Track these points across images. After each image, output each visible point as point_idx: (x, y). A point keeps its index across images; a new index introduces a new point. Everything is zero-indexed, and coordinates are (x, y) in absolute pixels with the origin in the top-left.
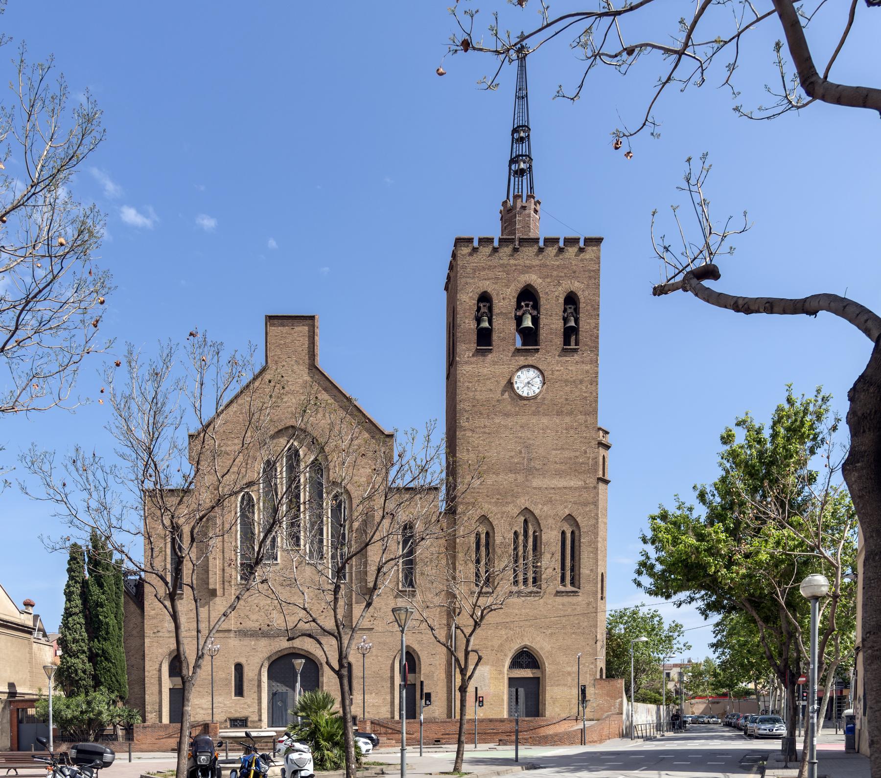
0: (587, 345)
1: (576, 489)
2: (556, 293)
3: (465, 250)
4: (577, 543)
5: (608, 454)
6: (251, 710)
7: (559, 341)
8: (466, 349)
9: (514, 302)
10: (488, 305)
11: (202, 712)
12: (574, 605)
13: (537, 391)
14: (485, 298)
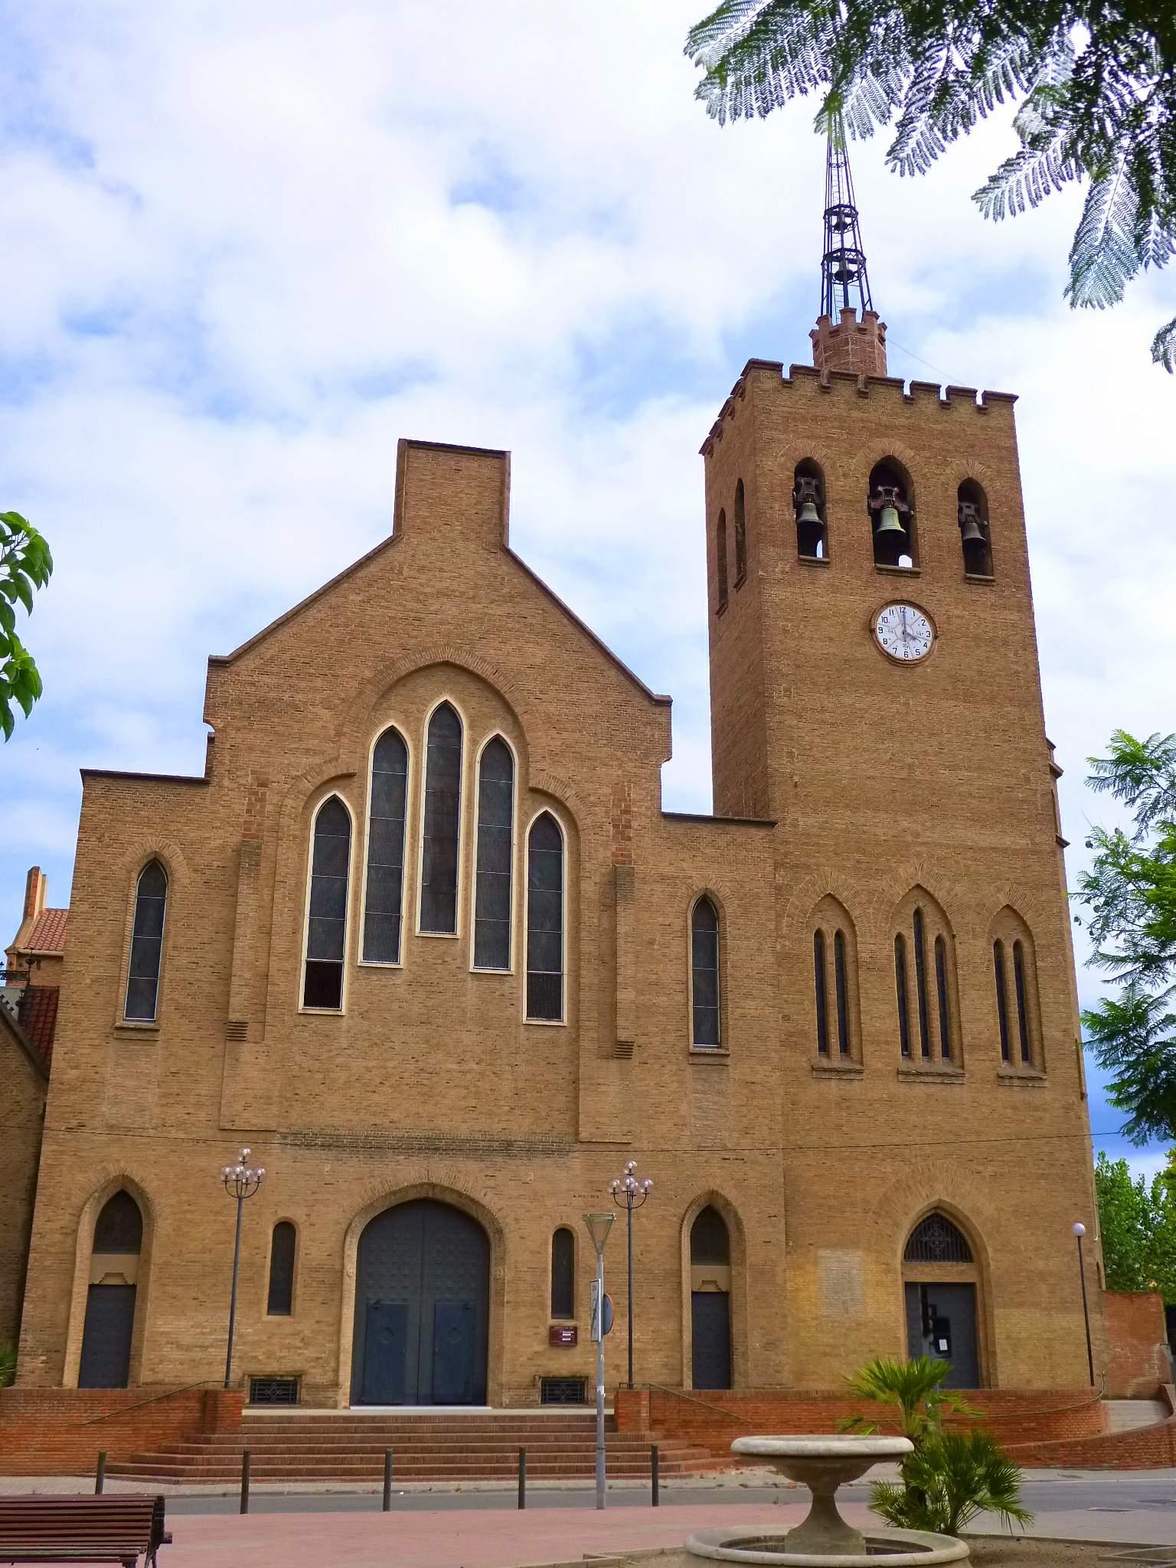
1: (1016, 852)
3: (767, 381)
4: (1029, 971)
6: (311, 1352)
7: (956, 562)
8: (776, 558)
9: (864, 483)
11: (177, 1355)
12: (1036, 1109)
13: (924, 651)
14: (807, 470)
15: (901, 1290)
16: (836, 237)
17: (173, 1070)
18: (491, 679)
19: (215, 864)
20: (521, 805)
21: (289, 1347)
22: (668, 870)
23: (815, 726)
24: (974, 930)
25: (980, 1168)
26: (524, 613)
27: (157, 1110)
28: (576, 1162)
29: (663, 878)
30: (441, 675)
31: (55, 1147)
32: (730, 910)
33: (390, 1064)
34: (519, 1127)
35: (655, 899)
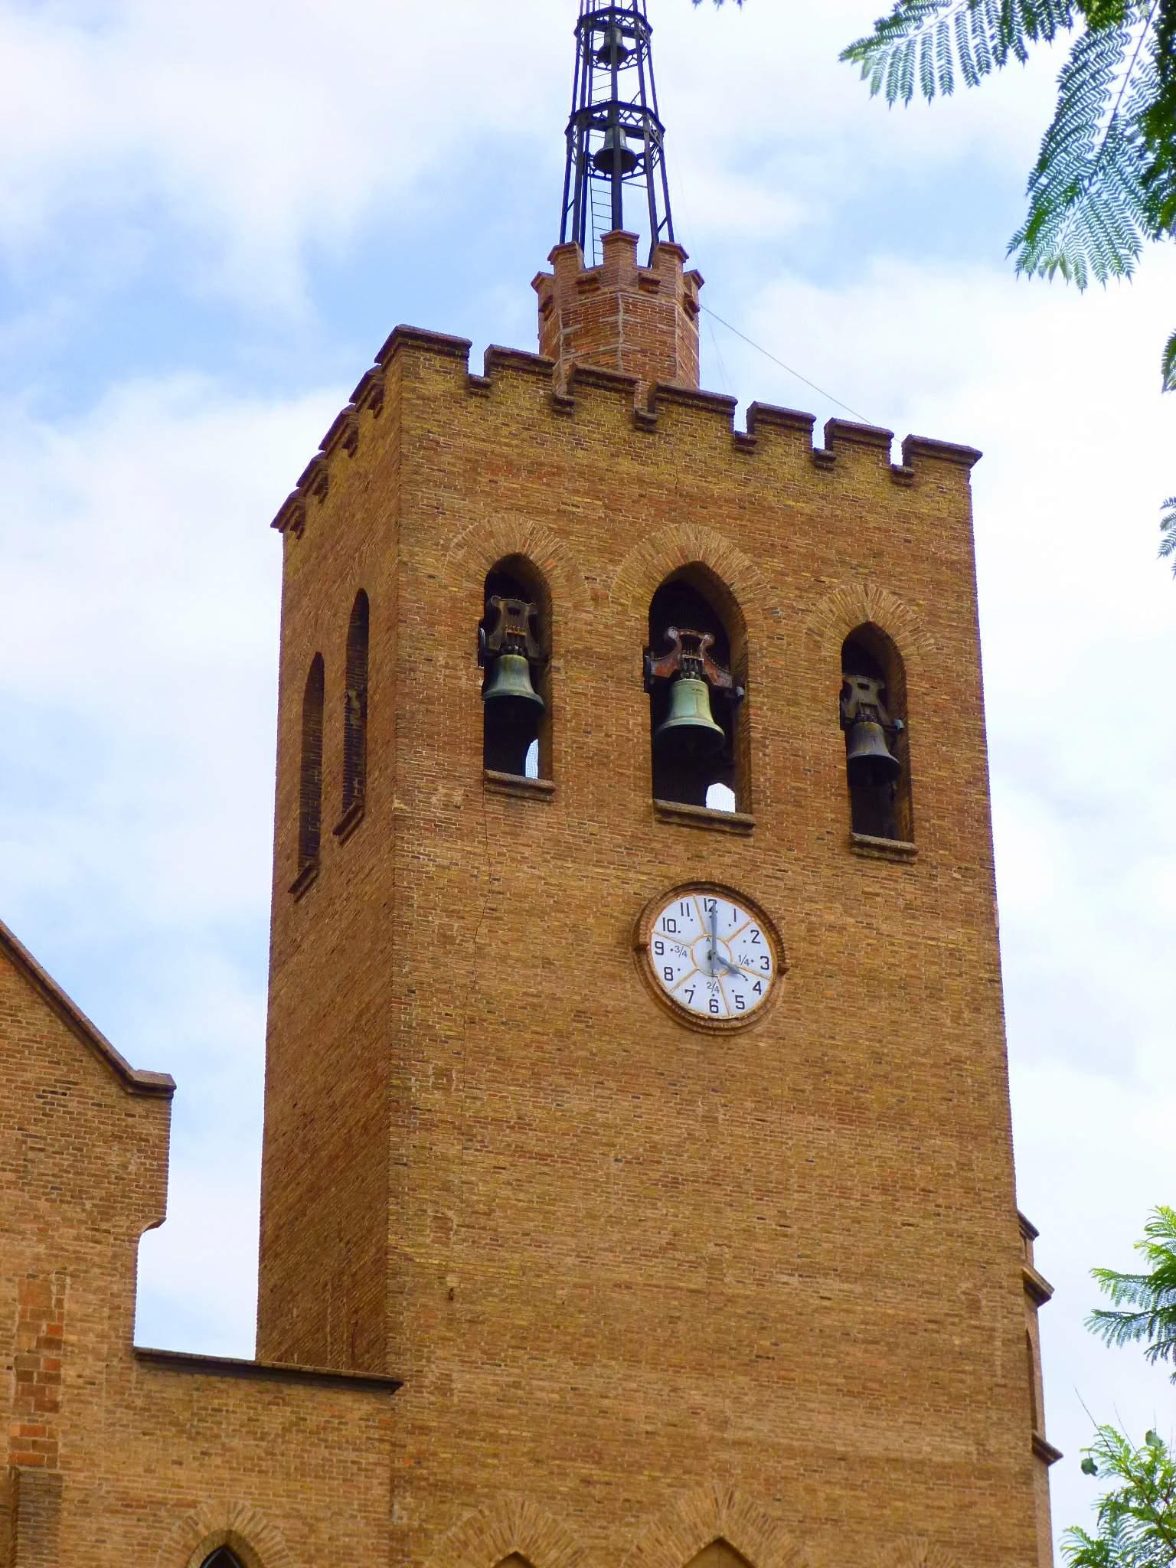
0: (943, 844)
1: (943, 1472)
2: (811, 620)
5: (1134, 1340)
7: (832, 808)
8: (432, 773)
9: (638, 618)
10: (527, 610)
13: (753, 1000)
14: (513, 581)
22: (139, 1486)
23: (502, 1160)
29: (128, 1504)
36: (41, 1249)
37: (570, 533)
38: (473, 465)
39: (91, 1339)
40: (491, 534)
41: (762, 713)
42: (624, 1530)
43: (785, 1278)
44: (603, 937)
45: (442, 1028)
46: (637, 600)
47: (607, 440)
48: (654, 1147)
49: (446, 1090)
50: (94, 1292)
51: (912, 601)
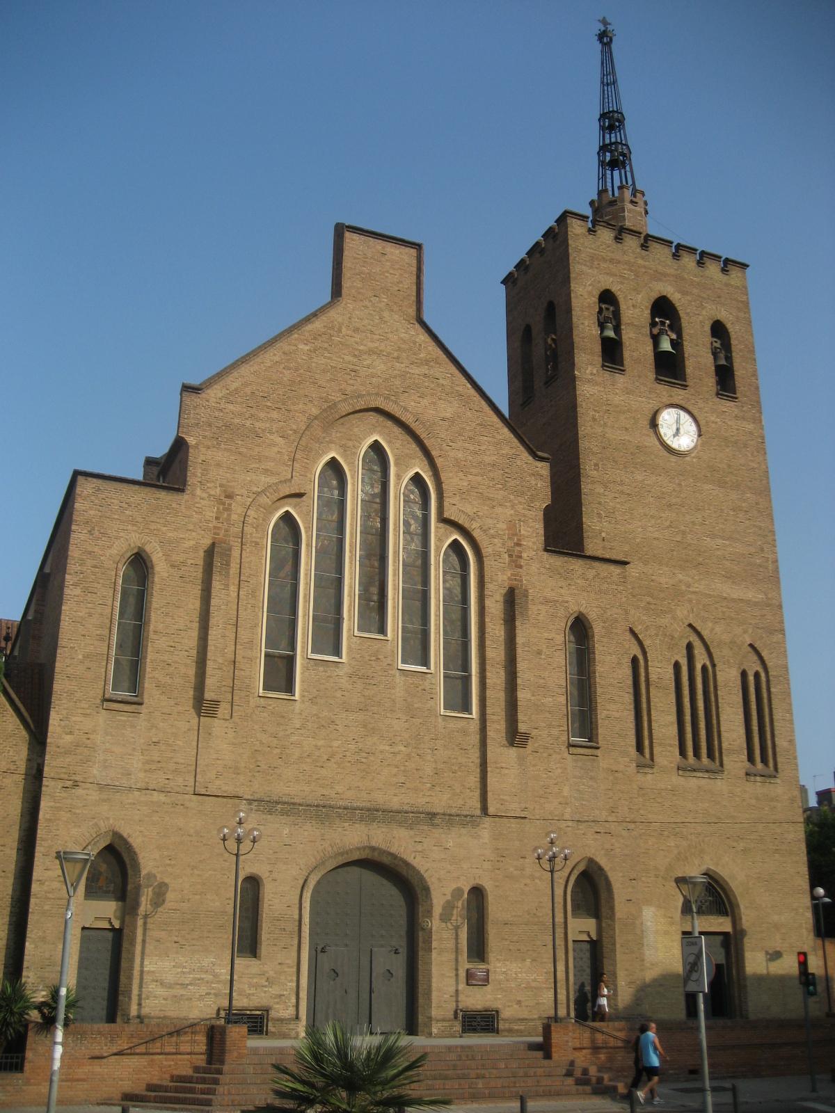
1: (756, 604)
6: (275, 990)
7: (710, 381)
9: (647, 313)
11: (160, 991)
14: (607, 298)
15: (679, 936)
16: (607, 136)
17: (154, 740)
18: (413, 426)
19: (190, 562)
20: (436, 532)
21: (256, 986)
22: (549, 594)
23: (617, 495)
24: (728, 661)
25: (735, 844)
26: (437, 375)
27: (141, 775)
28: (486, 829)
29: (547, 601)
30: (373, 418)
31: (52, 804)
32: (598, 629)
33: (336, 744)
34: (440, 801)
35: (541, 618)
36: (512, 512)
37: (624, 283)
38: (592, 258)
39: (530, 544)
40: (599, 282)
41: (688, 349)
42: (661, 620)
43: (705, 538)
44: (645, 422)
45: (595, 449)
46: (646, 307)
47: (633, 252)
48: (663, 493)
49: (597, 470)
50: (530, 528)
51: (731, 314)
